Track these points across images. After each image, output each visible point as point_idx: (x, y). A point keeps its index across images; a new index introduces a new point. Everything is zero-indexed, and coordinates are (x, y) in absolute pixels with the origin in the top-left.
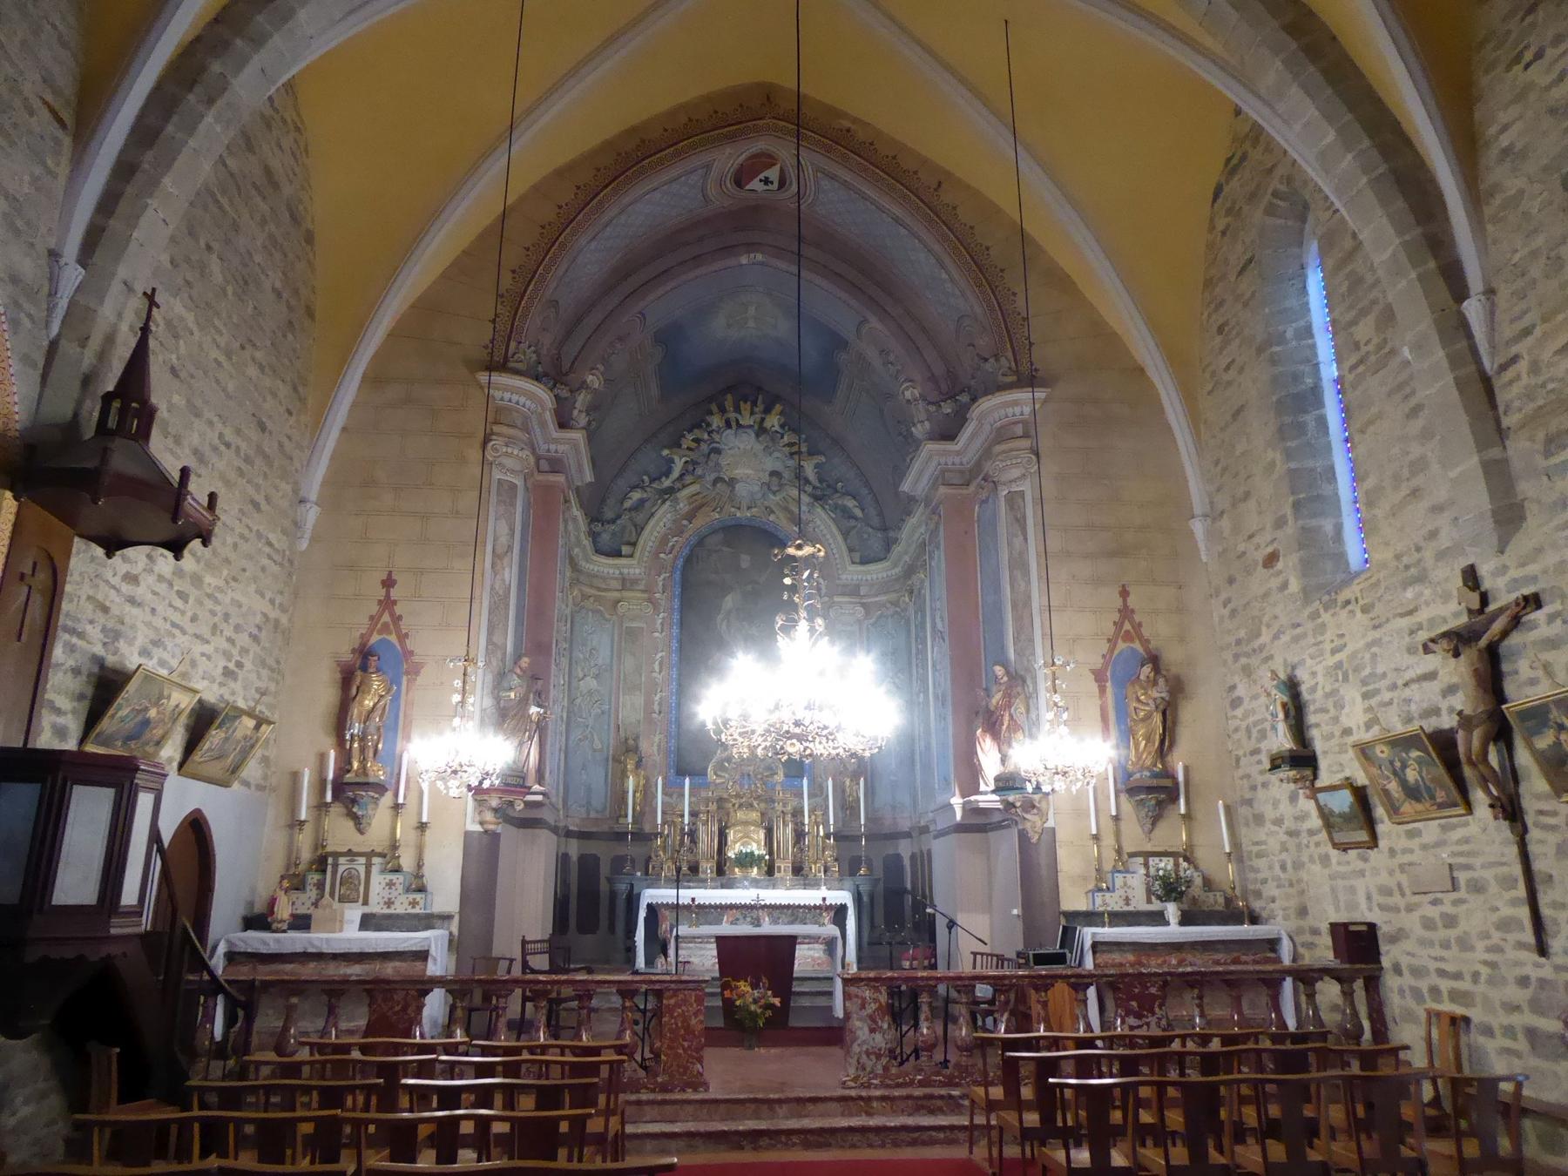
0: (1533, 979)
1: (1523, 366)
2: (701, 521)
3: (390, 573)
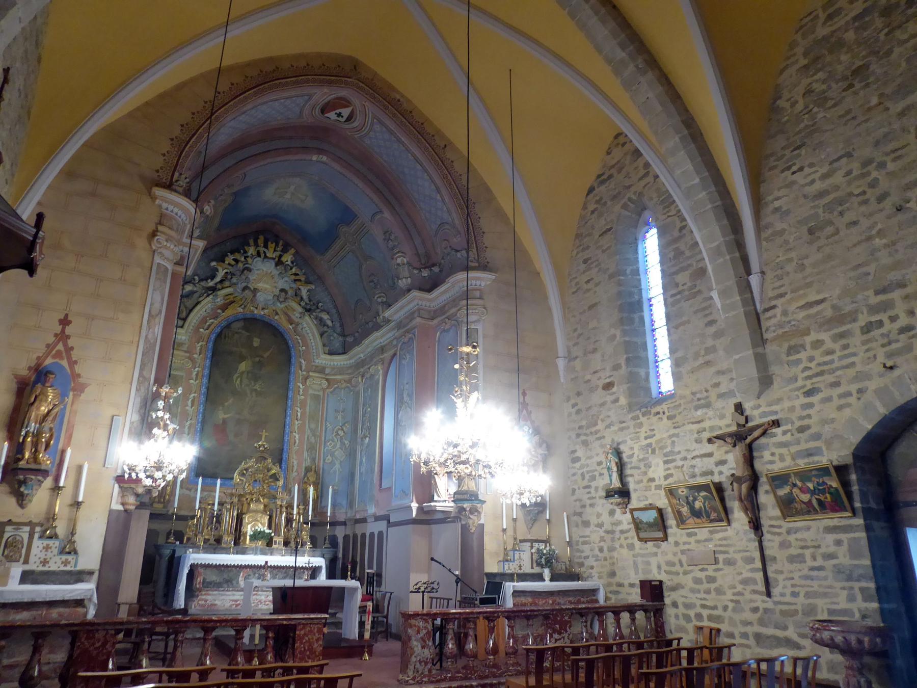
0: (761, 609)
1: (778, 311)
2: (230, 312)
3: (67, 315)
